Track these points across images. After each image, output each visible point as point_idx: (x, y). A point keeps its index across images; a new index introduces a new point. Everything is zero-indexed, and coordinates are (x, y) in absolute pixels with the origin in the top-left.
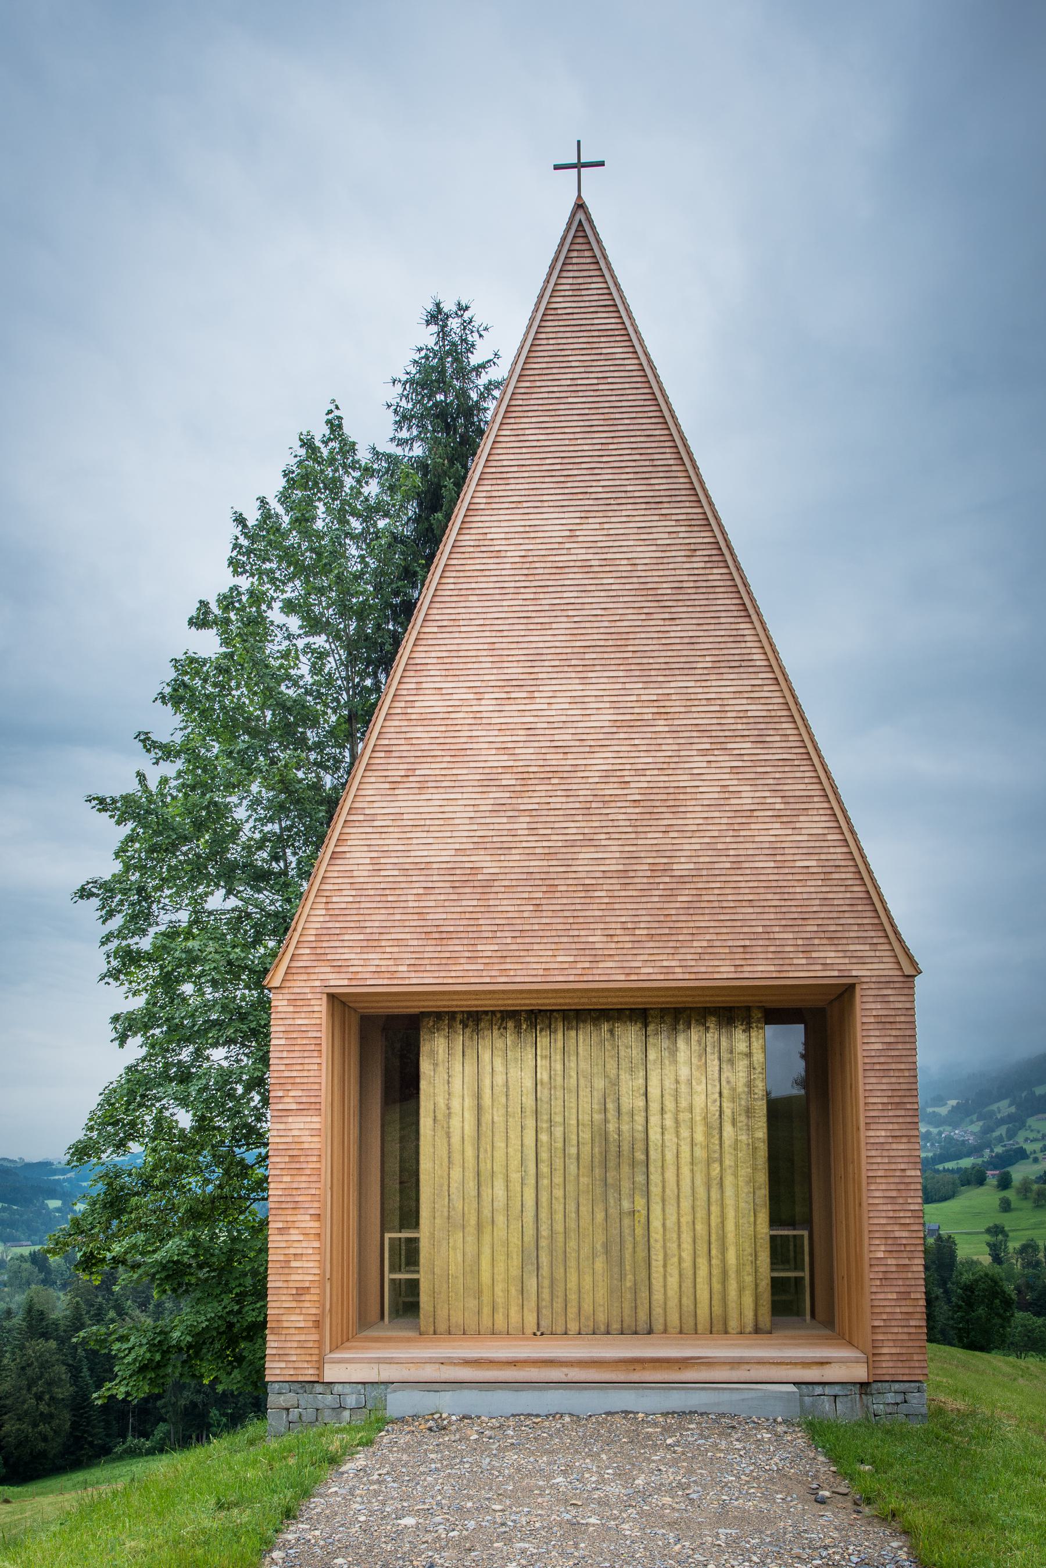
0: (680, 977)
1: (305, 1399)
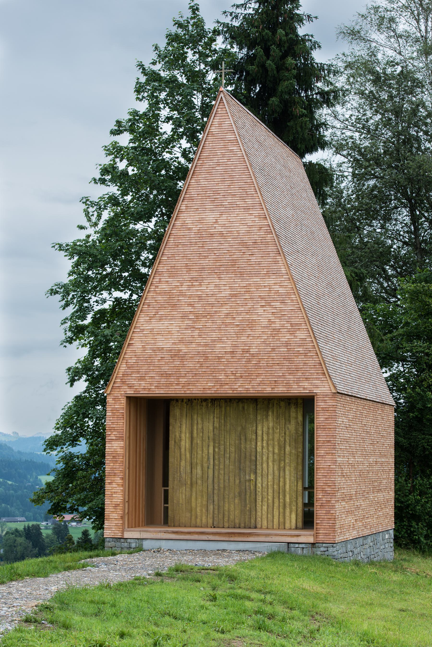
0: (252, 392)
1: (118, 544)
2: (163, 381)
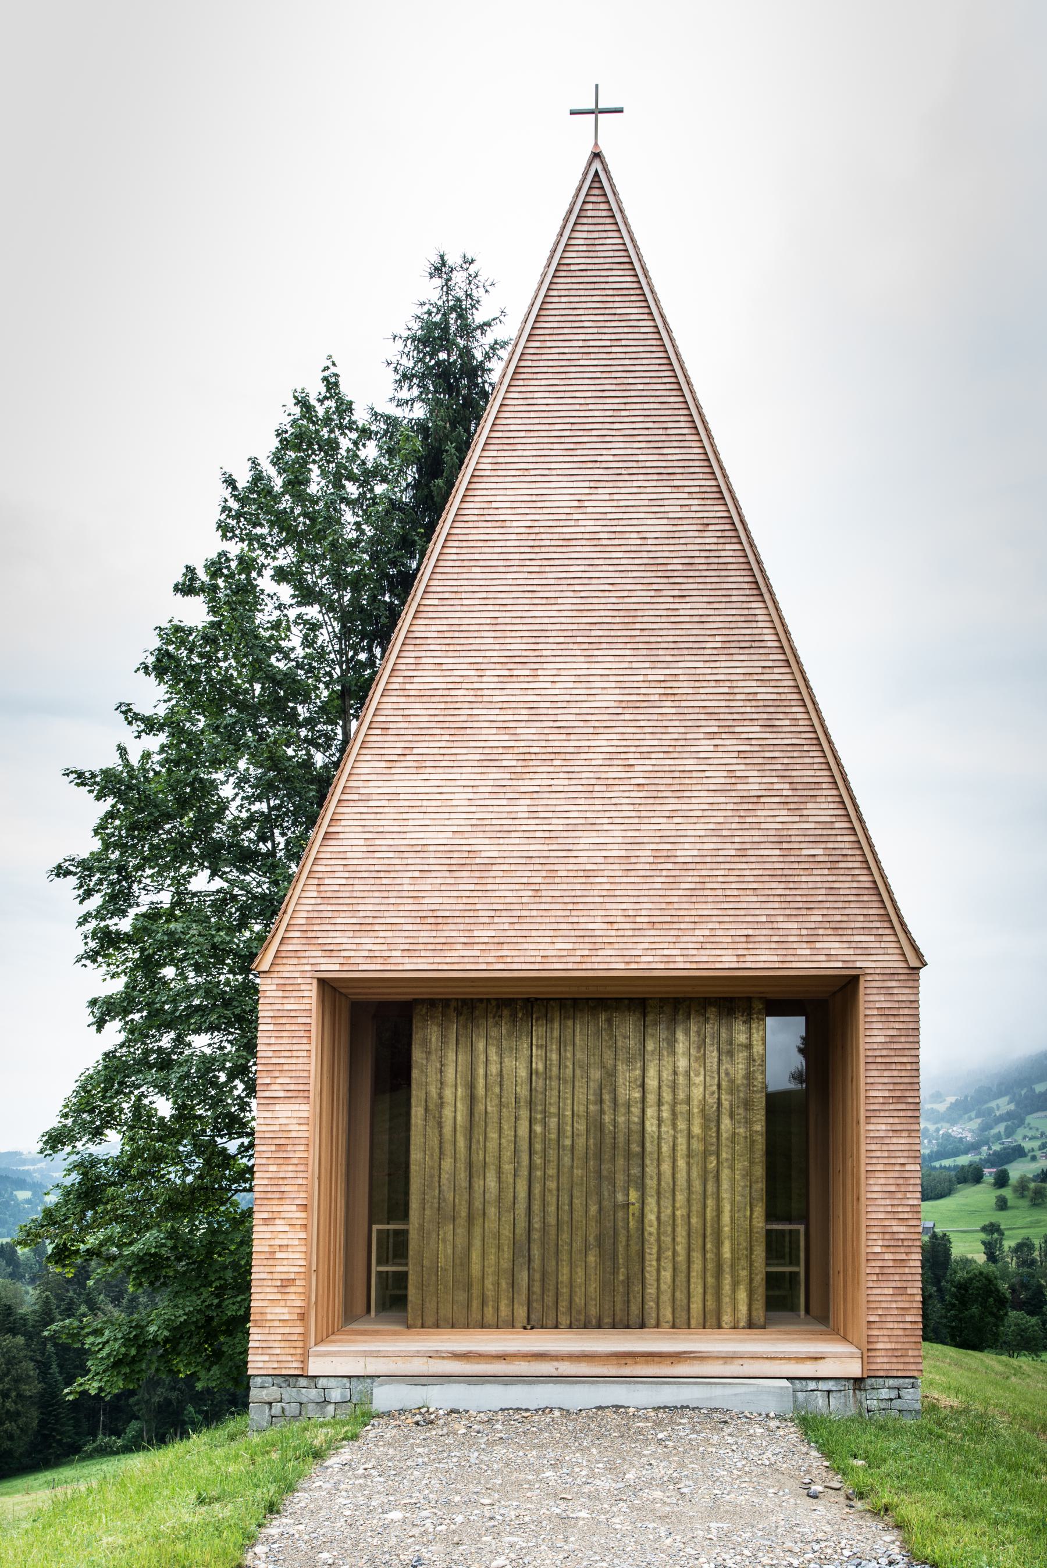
1: (289, 1393)
2: (425, 934)
